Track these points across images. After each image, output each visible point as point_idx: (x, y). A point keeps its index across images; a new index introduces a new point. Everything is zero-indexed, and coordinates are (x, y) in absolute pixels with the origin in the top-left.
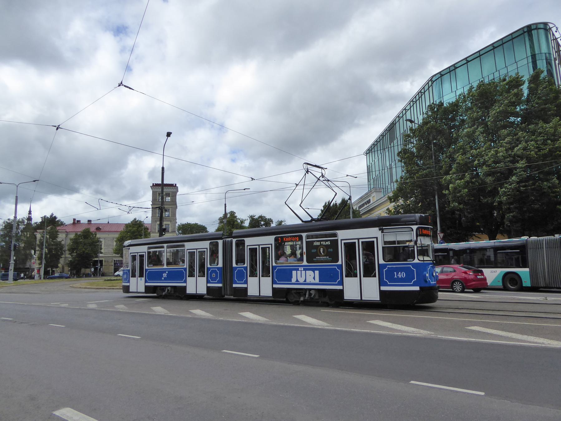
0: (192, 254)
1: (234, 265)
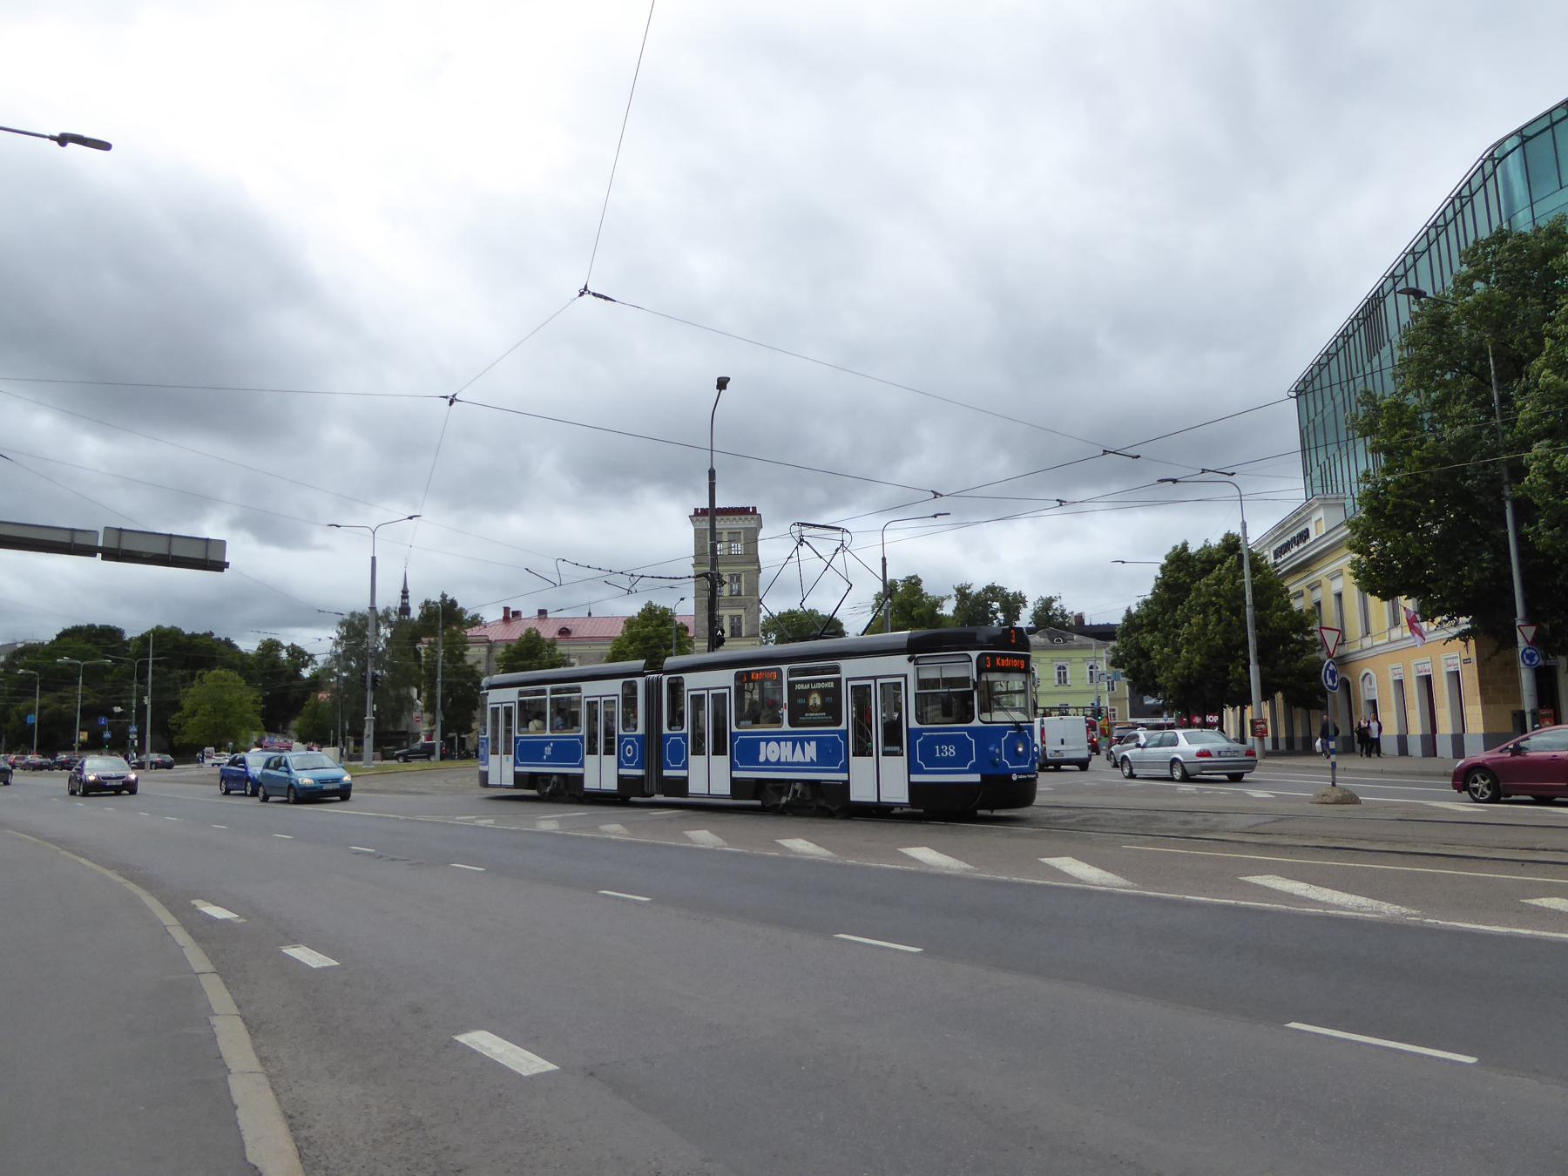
0: (861, 694)
1: (665, 730)
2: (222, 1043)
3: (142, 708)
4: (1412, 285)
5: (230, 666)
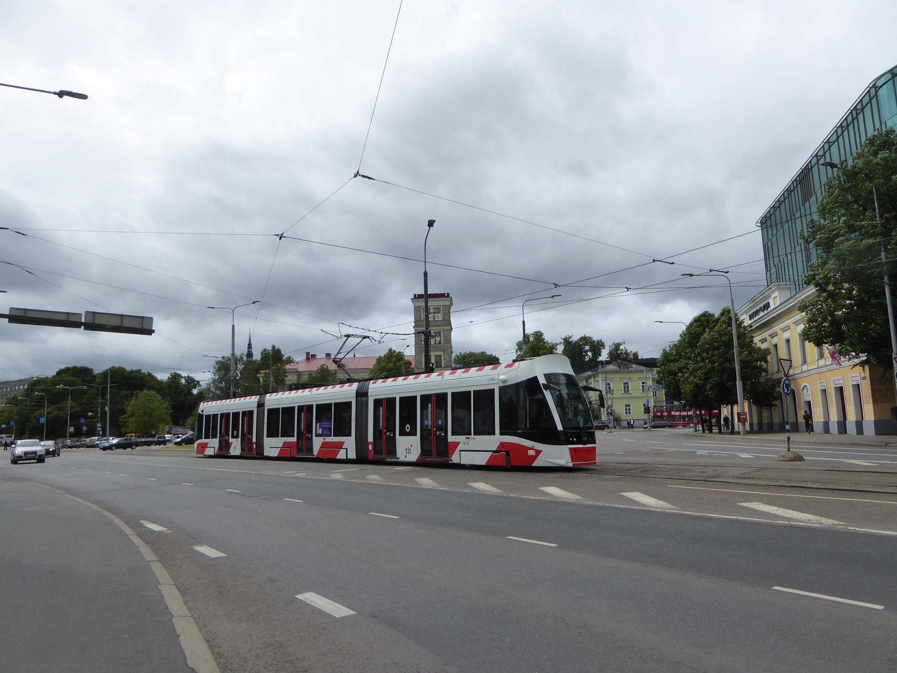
2: (167, 599)
3: (104, 413)
4: (828, 160)
5: (154, 389)
